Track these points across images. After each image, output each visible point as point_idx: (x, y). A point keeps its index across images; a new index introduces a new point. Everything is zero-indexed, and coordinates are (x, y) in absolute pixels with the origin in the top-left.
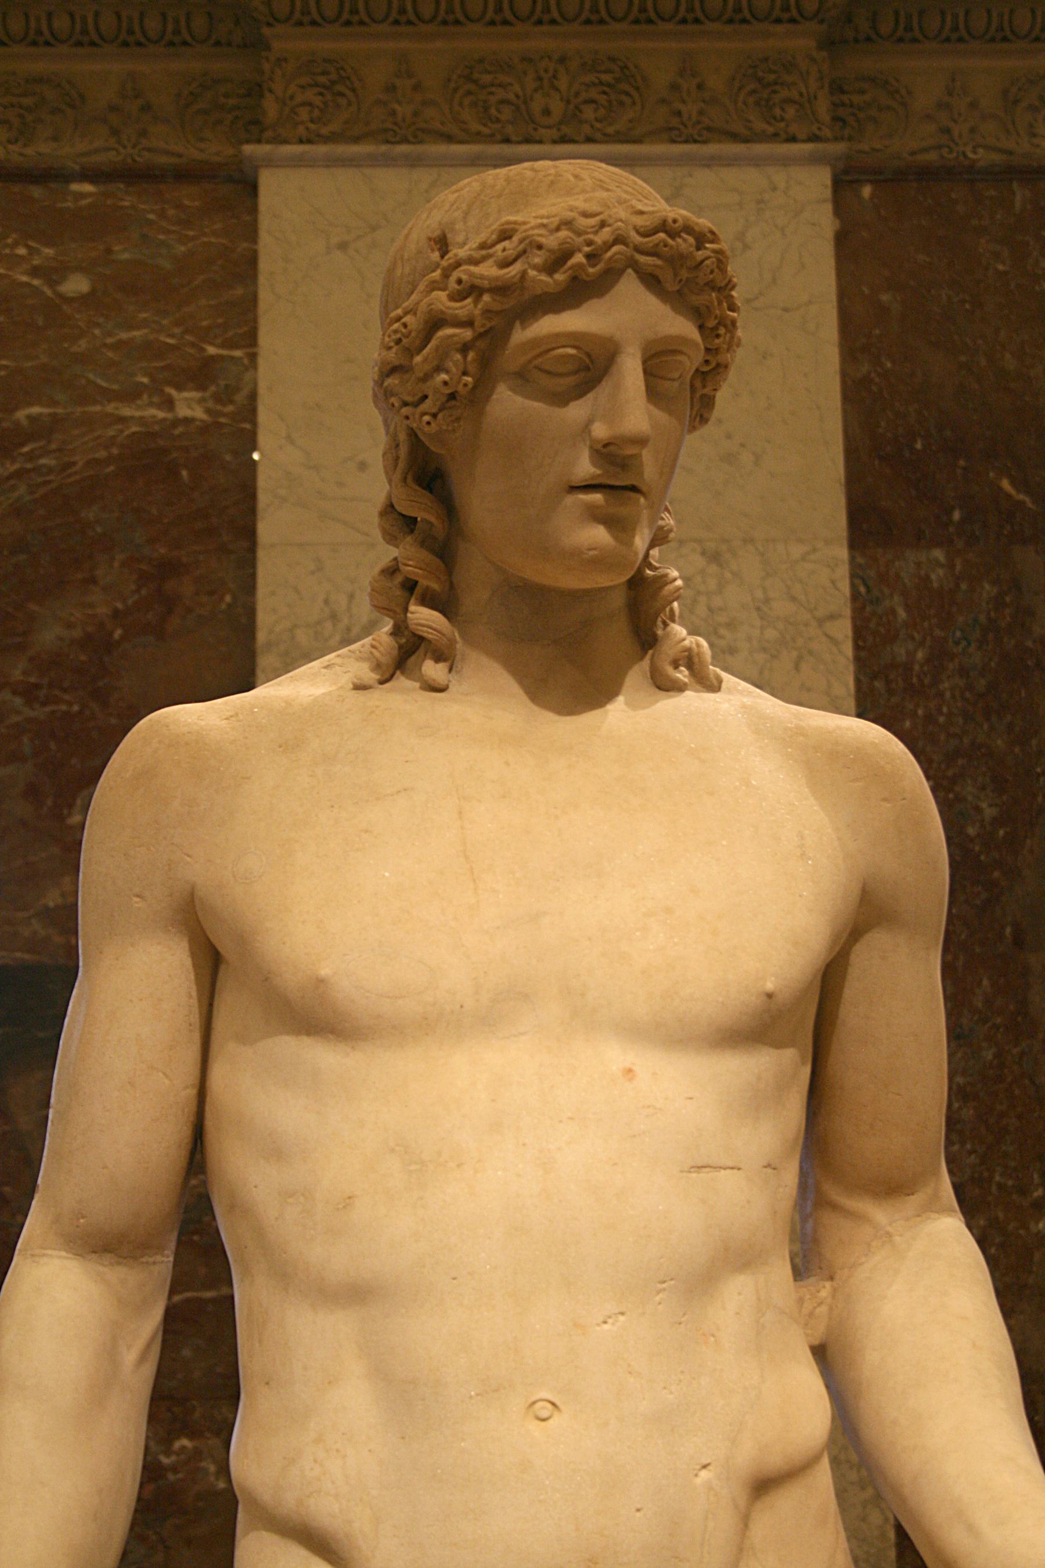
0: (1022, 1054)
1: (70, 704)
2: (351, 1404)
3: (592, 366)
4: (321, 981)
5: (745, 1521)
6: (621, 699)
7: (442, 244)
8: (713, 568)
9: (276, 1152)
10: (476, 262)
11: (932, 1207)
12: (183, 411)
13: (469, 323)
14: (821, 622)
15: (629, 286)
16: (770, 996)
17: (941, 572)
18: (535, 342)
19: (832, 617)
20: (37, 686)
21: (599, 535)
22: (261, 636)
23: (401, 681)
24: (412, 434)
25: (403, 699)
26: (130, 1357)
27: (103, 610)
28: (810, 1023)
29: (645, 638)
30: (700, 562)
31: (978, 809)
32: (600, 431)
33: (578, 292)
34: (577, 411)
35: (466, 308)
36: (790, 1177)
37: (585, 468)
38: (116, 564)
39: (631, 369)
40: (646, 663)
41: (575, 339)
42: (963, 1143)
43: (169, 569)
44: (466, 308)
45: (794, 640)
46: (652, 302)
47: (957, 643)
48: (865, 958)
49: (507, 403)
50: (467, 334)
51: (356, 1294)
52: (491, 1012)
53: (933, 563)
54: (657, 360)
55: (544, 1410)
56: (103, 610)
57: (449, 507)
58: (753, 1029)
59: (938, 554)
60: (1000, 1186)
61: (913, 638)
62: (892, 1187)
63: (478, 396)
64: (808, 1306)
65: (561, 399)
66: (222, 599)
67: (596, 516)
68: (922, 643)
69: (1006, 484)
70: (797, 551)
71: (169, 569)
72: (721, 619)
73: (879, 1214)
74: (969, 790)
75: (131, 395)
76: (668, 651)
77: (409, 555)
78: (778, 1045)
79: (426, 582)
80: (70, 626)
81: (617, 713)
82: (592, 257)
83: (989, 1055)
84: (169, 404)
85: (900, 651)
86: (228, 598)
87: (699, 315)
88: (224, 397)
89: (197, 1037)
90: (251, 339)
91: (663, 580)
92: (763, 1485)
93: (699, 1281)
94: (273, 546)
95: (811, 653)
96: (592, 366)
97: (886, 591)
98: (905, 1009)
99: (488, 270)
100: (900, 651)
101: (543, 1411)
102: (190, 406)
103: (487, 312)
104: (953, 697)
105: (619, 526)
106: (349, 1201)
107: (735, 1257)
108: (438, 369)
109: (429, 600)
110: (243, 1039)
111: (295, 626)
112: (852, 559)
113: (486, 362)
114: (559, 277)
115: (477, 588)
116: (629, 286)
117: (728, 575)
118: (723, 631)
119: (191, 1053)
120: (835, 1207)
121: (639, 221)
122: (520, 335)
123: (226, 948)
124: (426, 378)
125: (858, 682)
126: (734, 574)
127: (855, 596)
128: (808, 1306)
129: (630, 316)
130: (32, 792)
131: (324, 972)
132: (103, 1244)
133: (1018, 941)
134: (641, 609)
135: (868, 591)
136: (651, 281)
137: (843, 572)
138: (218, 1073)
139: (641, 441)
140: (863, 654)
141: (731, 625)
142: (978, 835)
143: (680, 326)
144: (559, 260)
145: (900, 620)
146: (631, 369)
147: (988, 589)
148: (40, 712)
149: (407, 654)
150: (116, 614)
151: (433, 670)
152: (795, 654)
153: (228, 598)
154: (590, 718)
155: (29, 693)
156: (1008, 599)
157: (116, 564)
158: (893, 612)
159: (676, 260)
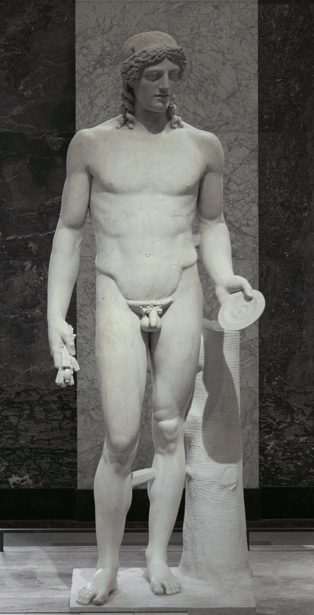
0: (304, 163)
1: (18, 51)
2: (116, 254)
3: (159, 75)
4: (111, 184)
5: (181, 274)
6: (164, 131)
7: (133, 50)
8: (216, 11)
9: (103, 212)
10: (139, 57)
11: (220, 221)
13: (137, 67)
14: (248, 29)
15: (166, 60)
17: (287, 12)
19: (252, 27)
20: (9, 46)
21: (160, 104)
22: (77, 32)
23: (125, 127)
24: (128, 84)
25: (125, 131)
26: (77, 246)
27: (28, 21)
28: (197, 191)
29: (169, 118)
30: (212, 9)
31: (294, 88)
32: (160, 86)
33: (157, 63)
34: (156, 83)
35: (136, 65)
36: (192, 217)
37: (158, 93)
38: (32, 6)
39: (166, 75)
40: (169, 123)
41: (156, 71)
42: (284, 190)
44: (136, 65)
45: (240, 34)
46: (170, 63)
47: (291, 35)
48: (208, 178)
49: (144, 81)
50: (137, 69)
51: (117, 236)
52: (139, 190)
54: (171, 73)
55: (148, 255)
56: (28, 21)
58: (186, 192)
59: (286, 6)
60: (295, 202)
61: (277, 33)
62: (212, 218)
63: (139, 79)
64: (196, 239)
65: (153, 81)
66: (64, 18)
68: (280, 35)
70: (242, 5)
72: (218, 27)
73: (210, 223)
76: (174, 121)
77: (127, 105)
78: (190, 194)
79: (129, 109)
80: (18, 26)
81: (163, 134)
83: (293, 163)
85: (273, 37)
86: (66, 18)
87: (179, 64)
89: (89, 191)
91: (173, 108)
92: (184, 268)
94: (80, 2)
95: (245, 39)
96: (159, 75)
97: (270, 18)
98: (215, 186)
99: (141, 59)
100: (273, 37)
103: (141, 66)
104: (289, 52)
105: (164, 102)
106: (116, 221)
107: (181, 231)
108: (132, 74)
109: (130, 112)
110: (97, 192)
111: (87, 28)
112: (259, 7)
113: (140, 73)
116: (166, 60)
117: (221, 14)
118: (218, 31)
119: (88, 194)
120: (202, 222)
121: (168, 49)
123: (94, 175)
124: (130, 75)
125: (259, 47)
126: (223, 13)
127: (259, 19)
128: (196, 239)
129: (166, 66)
130: (8, 79)
131: (112, 182)
132: (73, 227)
135: (264, 18)
136: (170, 59)
137: (256, 12)
138: (93, 198)
139: (168, 89)
140: (261, 38)
141: (221, 30)
142: (294, 96)
143: (176, 67)
144: (154, 57)
145: (273, 27)
146: (166, 75)
149: (126, 122)
150: (32, 22)
151: (131, 125)
152: (240, 39)
153: (66, 18)
154: (159, 134)
155: (6, 47)
156: (307, 21)
157: (32, 6)
158: (272, 24)
159: (174, 56)
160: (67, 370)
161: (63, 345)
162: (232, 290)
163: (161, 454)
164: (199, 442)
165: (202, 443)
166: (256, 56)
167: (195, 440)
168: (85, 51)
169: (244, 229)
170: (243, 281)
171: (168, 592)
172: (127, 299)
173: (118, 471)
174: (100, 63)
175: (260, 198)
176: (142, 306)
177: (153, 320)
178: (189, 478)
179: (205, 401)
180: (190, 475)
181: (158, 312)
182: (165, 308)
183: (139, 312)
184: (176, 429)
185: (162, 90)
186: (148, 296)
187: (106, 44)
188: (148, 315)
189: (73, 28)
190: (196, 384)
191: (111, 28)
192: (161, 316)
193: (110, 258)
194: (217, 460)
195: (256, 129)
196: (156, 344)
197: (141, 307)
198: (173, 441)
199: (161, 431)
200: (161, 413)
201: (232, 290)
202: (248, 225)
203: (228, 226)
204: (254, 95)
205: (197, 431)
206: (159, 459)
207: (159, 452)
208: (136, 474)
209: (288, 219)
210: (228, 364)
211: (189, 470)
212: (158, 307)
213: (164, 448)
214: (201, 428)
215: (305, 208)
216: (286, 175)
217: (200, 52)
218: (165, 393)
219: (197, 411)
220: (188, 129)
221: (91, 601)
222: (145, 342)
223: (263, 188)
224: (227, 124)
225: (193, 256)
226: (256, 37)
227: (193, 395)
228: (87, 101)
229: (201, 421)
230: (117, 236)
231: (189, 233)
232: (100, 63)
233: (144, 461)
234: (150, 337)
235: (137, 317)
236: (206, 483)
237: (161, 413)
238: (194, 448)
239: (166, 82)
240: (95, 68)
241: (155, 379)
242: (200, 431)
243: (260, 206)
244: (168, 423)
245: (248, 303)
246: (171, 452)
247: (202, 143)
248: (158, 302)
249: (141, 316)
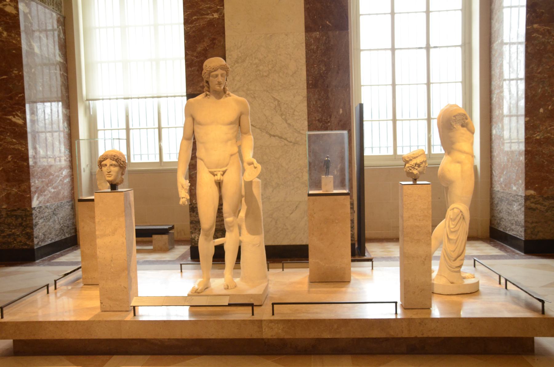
3: (217, 76)
12: (215, 16)
21: (218, 88)
25: (206, 99)
28: (238, 122)
33: (215, 71)
39: (220, 76)
43: (214, 39)
49: (211, 78)
51: (203, 143)
53: (317, 34)
56: (206, 45)
57: (209, 84)
58: (231, 123)
59: (318, 33)
63: (209, 77)
69: (327, 22)
71: (214, 39)
73: (245, 136)
74: (321, 66)
75: (208, 14)
81: (222, 100)
83: (323, 102)
84: (213, 15)
85: (312, 47)
88: (220, 14)
90: (223, 5)
92: (231, 155)
93: (226, 141)
96: (217, 76)
100: (312, 47)
102: (216, 16)
127: (306, 39)
129: (219, 72)
133: (327, 87)
134: (224, 91)
143: (224, 72)
146: (220, 76)
147: (325, 38)
148: (198, 60)
155: (197, 57)
162: (250, 164)
166: (305, 55)
168: (230, 57)
169: (302, 132)
170: (255, 161)
171: (229, 288)
173: (206, 239)
174: (237, 62)
175: (308, 118)
177: (219, 177)
182: (224, 172)
184: (233, 221)
185: (218, 82)
186: (216, 168)
187: (239, 53)
189: (225, 47)
191: (241, 47)
192: (223, 175)
195: (306, 87)
198: (232, 226)
201: (250, 164)
202: (303, 130)
204: (304, 73)
209: (321, 126)
211: (241, 238)
215: (329, 122)
216: (320, 107)
217: (280, 55)
219: (242, 214)
220: (234, 96)
221: (196, 292)
223: (309, 114)
224: (292, 86)
225: (236, 149)
226: (304, 47)
228: (232, 78)
229: (244, 218)
231: (234, 141)
232: (237, 62)
234: (219, 184)
239: (220, 79)
240: (235, 64)
243: (309, 122)
245: (255, 170)
247: (238, 102)
248: (221, 170)
249: (214, 175)
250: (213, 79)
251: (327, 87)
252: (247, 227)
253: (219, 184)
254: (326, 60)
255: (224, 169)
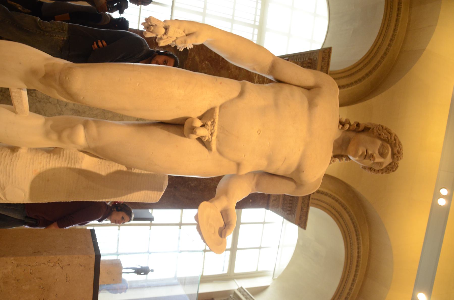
3: (382, 155)
4: (317, 106)
5: (234, 161)
16: (303, 172)
18: (388, 147)
33: (393, 154)
34: (377, 152)
37: (370, 152)
41: (387, 153)
49: (379, 142)
50: (389, 138)
51: (276, 105)
55: (259, 132)
58: (299, 170)
62: (257, 185)
63: (380, 139)
65: (379, 150)
67: (363, 153)
73: (254, 182)
74: (195, 182)
82: (397, 157)
101: (259, 132)
102: (256, 81)
114: (396, 152)
115: (352, 135)
122: (389, 145)
136: (390, 164)
144: (398, 152)
149: (342, 123)
159: (392, 168)
160: (163, 31)
161: (187, 33)
163: (45, 124)
164: (54, 163)
165: (53, 166)
167: (56, 159)
172: (221, 107)
173: (33, 72)
176: (213, 122)
178: (14, 149)
179: (98, 172)
180: (18, 151)
181: (205, 137)
183: (207, 117)
184: (73, 142)
186: (222, 128)
188: (203, 126)
190: (114, 163)
192: (200, 139)
193: (256, 95)
194: (34, 182)
196: (169, 131)
197: (213, 120)
198: (60, 138)
199: (72, 127)
200: (93, 129)
203: (261, 204)
205: (67, 162)
206: (38, 121)
207: (46, 121)
208: (25, 94)
210: (132, 194)
211: (23, 151)
212: (210, 137)
213: (52, 127)
214: (69, 166)
218: (115, 134)
219: (88, 163)
222: (173, 120)
227: (102, 159)
229: (78, 166)
230: (276, 105)
233: (38, 104)
234: (179, 126)
235: (200, 114)
236: (8, 169)
237: (93, 129)
238: (47, 157)
241: (129, 125)
242: (66, 165)
244: (81, 137)
246: (47, 134)
248: (214, 138)
250: (378, 147)
251: (175, 187)
252: (54, 171)
253: (179, 126)
254: (201, 187)
255: (214, 146)
